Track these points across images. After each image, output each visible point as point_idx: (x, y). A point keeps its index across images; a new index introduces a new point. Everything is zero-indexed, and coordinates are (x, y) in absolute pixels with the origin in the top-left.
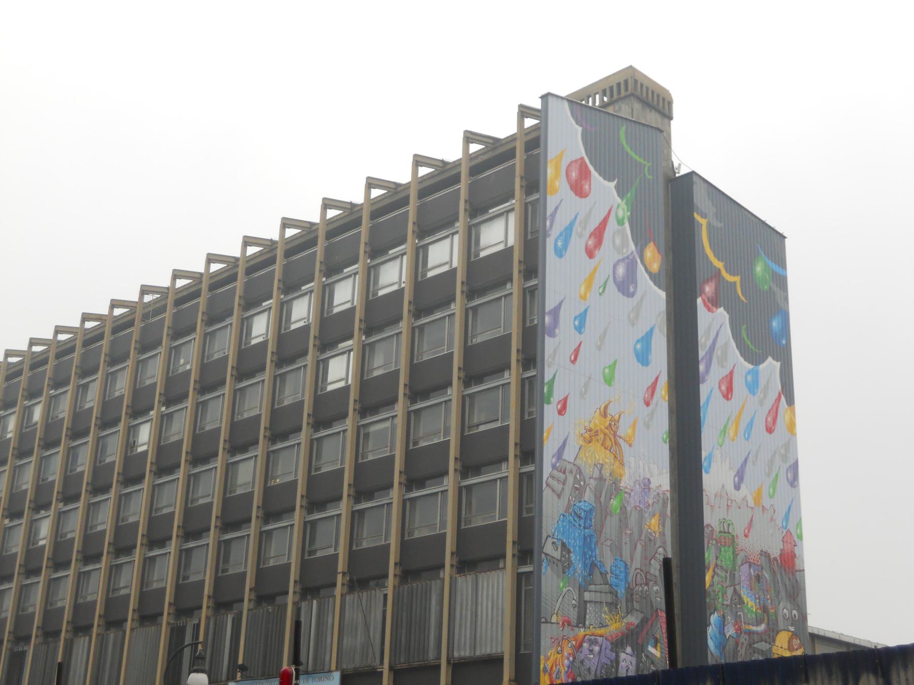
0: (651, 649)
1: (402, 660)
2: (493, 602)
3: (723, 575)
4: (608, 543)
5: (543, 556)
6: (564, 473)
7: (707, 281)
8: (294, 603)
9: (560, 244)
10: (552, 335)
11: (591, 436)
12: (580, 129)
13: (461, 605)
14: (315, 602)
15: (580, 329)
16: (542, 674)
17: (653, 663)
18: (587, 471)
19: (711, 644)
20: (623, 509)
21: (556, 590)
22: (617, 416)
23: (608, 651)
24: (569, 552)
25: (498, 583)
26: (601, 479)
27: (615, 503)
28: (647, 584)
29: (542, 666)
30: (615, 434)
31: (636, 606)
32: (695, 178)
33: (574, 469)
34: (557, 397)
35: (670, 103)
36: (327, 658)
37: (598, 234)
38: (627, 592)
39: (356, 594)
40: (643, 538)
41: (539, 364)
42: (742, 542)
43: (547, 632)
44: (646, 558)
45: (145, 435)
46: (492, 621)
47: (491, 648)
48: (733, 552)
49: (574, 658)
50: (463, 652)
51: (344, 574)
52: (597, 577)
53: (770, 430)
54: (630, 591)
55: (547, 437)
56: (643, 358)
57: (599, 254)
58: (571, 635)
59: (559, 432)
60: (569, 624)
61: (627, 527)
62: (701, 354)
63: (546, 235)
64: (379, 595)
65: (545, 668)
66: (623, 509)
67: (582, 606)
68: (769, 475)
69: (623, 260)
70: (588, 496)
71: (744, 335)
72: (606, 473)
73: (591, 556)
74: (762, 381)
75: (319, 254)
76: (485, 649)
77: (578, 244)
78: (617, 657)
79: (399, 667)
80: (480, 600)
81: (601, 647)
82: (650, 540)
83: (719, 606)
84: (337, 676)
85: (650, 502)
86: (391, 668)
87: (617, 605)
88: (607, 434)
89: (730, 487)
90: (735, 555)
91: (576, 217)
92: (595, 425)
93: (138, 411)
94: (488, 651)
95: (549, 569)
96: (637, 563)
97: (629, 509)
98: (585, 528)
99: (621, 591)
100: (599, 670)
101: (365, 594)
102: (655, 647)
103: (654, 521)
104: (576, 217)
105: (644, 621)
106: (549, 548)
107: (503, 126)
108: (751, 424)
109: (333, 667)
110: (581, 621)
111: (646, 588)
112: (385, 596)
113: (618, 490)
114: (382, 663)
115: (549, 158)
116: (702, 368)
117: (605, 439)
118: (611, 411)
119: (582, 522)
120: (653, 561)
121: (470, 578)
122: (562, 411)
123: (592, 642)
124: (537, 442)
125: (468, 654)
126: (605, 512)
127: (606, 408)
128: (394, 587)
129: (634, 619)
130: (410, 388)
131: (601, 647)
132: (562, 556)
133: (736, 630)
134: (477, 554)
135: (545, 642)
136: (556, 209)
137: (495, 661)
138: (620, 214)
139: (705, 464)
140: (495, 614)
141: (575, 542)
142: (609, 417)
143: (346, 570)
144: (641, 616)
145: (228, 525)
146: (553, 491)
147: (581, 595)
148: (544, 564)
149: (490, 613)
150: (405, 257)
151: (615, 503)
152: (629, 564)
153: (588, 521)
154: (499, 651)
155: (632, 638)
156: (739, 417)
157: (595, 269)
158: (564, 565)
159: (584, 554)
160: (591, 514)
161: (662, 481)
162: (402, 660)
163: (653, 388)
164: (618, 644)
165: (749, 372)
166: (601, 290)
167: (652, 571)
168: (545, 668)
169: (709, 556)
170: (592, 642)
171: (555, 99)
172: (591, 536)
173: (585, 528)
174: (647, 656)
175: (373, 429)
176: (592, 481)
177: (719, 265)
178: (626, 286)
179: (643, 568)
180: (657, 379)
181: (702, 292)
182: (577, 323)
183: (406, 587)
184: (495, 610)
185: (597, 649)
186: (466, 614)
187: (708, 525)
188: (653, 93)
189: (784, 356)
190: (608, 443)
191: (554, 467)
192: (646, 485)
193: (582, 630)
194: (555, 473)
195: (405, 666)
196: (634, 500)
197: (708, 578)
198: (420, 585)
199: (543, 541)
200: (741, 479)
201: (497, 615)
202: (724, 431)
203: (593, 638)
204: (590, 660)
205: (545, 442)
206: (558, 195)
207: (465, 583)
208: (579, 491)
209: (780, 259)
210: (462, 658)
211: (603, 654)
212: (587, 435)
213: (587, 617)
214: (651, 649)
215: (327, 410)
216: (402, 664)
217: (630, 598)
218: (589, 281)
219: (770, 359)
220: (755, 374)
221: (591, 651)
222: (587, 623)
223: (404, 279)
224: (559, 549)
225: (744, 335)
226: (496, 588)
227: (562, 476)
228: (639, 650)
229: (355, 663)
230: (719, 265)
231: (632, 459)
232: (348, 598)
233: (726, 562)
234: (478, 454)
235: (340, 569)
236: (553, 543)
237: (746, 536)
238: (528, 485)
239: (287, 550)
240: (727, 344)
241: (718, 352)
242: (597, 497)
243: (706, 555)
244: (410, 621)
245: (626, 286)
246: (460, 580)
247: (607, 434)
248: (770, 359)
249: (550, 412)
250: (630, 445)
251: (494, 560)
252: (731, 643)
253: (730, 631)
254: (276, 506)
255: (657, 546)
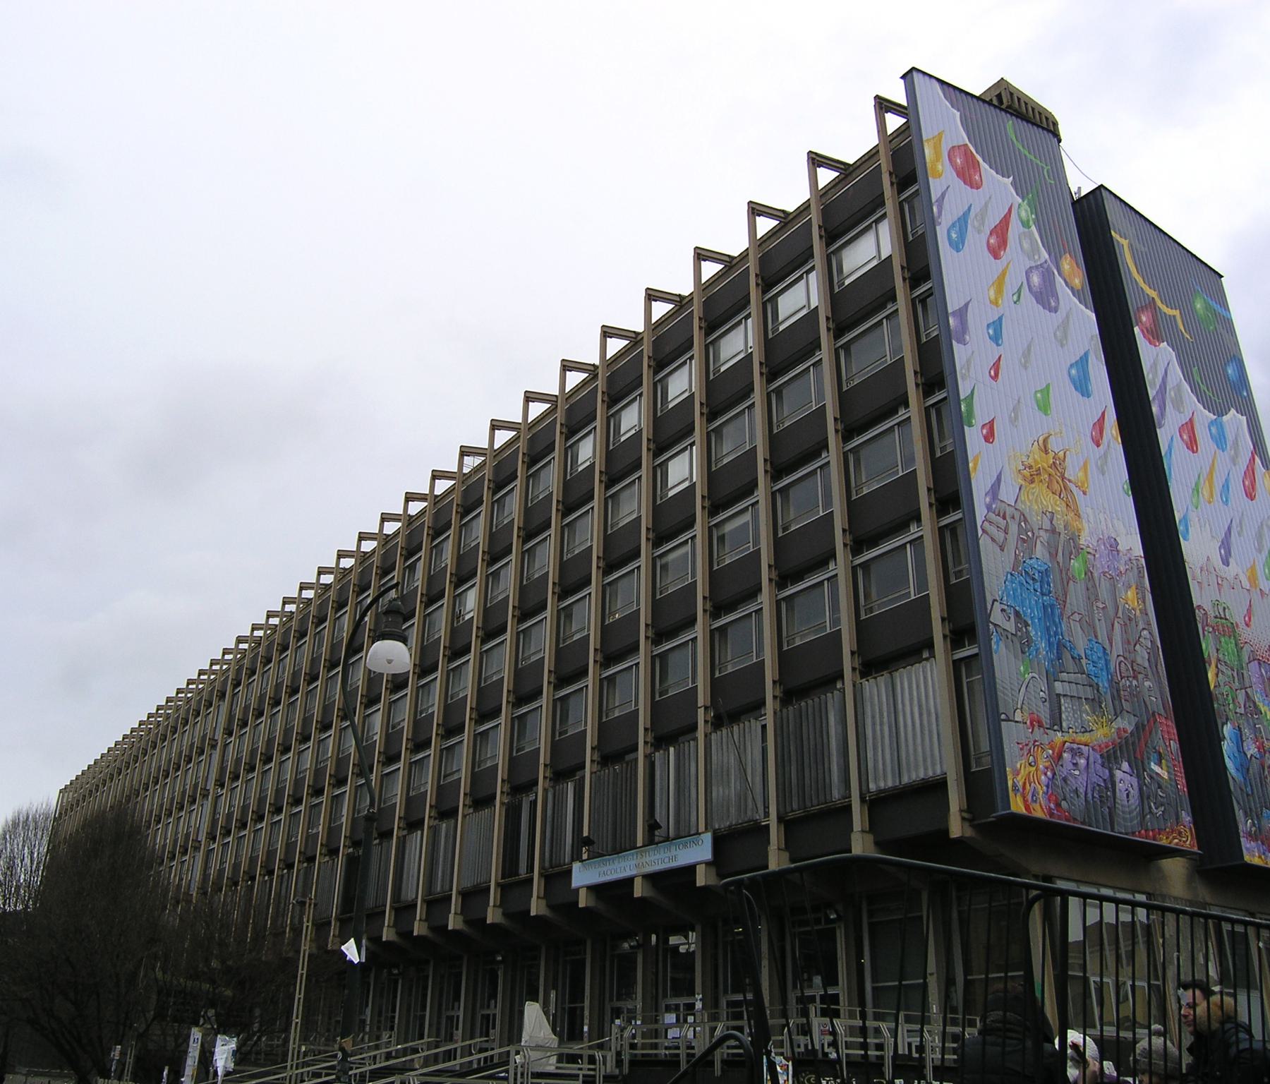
0: (1154, 767)
1: (795, 806)
2: (920, 706)
3: (1230, 673)
4: (1077, 617)
5: (991, 626)
6: (1004, 518)
7: (1142, 309)
8: (645, 756)
9: (954, 236)
10: (962, 341)
11: (1032, 475)
12: (958, 114)
13: (873, 717)
14: (672, 749)
15: (996, 338)
16: (1011, 794)
17: (1160, 787)
18: (1035, 520)
19: (1229, 764)
20: (1089, 573)
21: (1015, 674)
22: (1061, 454)
23: (1098, 767)
24: (1027, 625)
25: (925, 678)
26: (1053, 531)
27: (1076, 564)
28: (1135, 677)
29: (1010, 783)
30: (1063, 478)
31: (1126, 706)
32: (1104, 193)
33: (1017, 515)
34: (980, 418)
35: (1055, 124)
36: (693, 819)
37: (1001, 232)
38: (1111, 687)
39: (724, 731)
40: (1120, 614)
41: (949, 381)
42: (1244, 633)
43: (1012, 735)
44: (1129, 642)
45: (472, 600)
46: (922, 732)
47: (926, 769)
48: (1236, 645)
49: (1054, 774)
50: (883, 781)
51: (706, 708)
52: (1070, 665)
53: (1251, 495)
54: (1114, 685)
55: (975, 468)
56: (1082, 386)
57: (1007, 255)
58: (1046, 740)
59: (990, 467)
60: (1041, 726)
61: (1097, 599)
62: (1152, 393)
63: (933, 223)
64: (756, 726)
65: (1014, 785)
66: (1089, 573)
67: (1055, 701)
68: (1260, 551)
69: (1037, 267)
70: (1040, 551)
71: (1197, 378)
72: (1060, 526)
73: (1056, 633)
74: (1230, 437)
75: (645, 352)
76: (916, 773)
77: (977, 240)
78: (1112, 776)
79: (791, 816)
80: (900, 706)
81: (1088, 759)
82: (1130, 619)
83: (1231, 715)
84: (707, 838)
85: (1122, 569)
86: (780, 819)
87: (1100, 703)
88: (1049, 472)
89: (1217, 561)
90: (1239, 649)
91: (969, 209)
92: (1035, 461)
93: (463, 578)
94: (922, 776)
95: (1002, 645)
96: (1118, 648)
97: (1096, 575)
98: (1043, 594)
99: (1104, 684)
100: (1090, 795)
101: (736, 728)
102: (1160, 764)
103: (1131, 594)
104: (969, 209)
105: (1139, 727)
106: (997, 617)
107: (855, 139)
108: (1226, 486)
109: (702, 828)
110: (1056, 721)
111: (1135, 683)
112: (764, 727)
113: (1079, 549)
114: (767, 814)
115: (924, 138)
116: (1155, 409)
117: (1050, 480)
118: (1053, 445)
119: (1038, 585)
120: (1138, 647)
121: (883, 680)
122: (989, 437)
123: (1076, 753)
124: (962, 485)
125: (890, 784)
126: (1067, 578)
127: (1045, 441)
128: (775, 713)
129: (1126, 724)
130: (771, 463)
131: (1088, 759)
132: (1018, 629)
133: (1259, 748)
134: (889, 648)
135: (1010, 748)
136: (943, 195)
137: (936, 787)
138: (1023, 214)
139: (1181, 528)
140: (925, 722)
141: (1032, 612)
142: (1052, 454)
143: (709, 704)
144: (1134, 720)
145: (562, 680)
146: (993, 540)
147: (1050, 687)
148: (994, 640)
149: (918, 722)
150: (750, 321)
151: (1076, 564)
152: (1107, 646)
153: (1047, 583)
154: (939, 772)
155: (1128, 749)
156: (1211, 473)
157: (1003, 274)
158: (1025, 645)
159: (1048, 629)
160: (1048, 576)
161: (1132, 543)
162: (795, 806)
163: (1100, 424)
164: (1110, 757)
165: (1212, 423)
166: (1015, 298)
167: (1139, 661)
168: (1014, 785)
169: (1208, 645)
170: (1076, 753)
171: (921, 75)
172: (1052, 606)
173: (1043, 594)
174: (1151, 778)
175: (728, 527)
176: (1042, 533)
177: (1153, 294)
178: (1046, 297)
179: (1127, 655)
180: (1103, 414)
181: (1139, 322)
182: (991, 332)
183: (791, 708)
184: (925, 716)
185: (1082, 762)
186: (882, 730)
187: (1199, 607)
188: (1033, 109)
189: (1248, 408)
190: (1056, 487)
191: (989, 508)
192: (1113, 546)
193: (1059, 734)
194: (992, 516)
195: (799, 813)
196: (1101, 564)
197: (1211, 675)
198: (810, 702)
199: (989, 607)
200: (1228, 553)
201: (929, 722)
202: (1196, 490)
203: (1075, 746)
204: (1075, 777)
205: (973, 475)
206: (942, 180)
207: (875, 688)
208: (1027, 542)
209: (1219, 296)
210: (881, 791)
211: (1092, 770)
212: (1026, 472)
213: (1063, 716)
214: (1154, 767)
215: (670, 521)
216: (795, 810)
217: (1116, 696)
218: (1000, 282)
219: (1233, 411)
220: (1221, 427)
221: (1075, 765)
222: (1064, 724)
223: (750, 344)
224: (1012, 617)
225: (1197, 378)
226: (925, 685)
227: (1002, 523)
228: (1139, 768)
229: (731, 819)
230: (1153, 294)
231: (1089, 510)
232: (713, 736)
233: (1231, 659)
234: (876, 521)
235: (701, 703)
236: (1003, 610)
237: (1247, 625)
238: (957, 541)
239: (636, 693)
240: (1179, 386)
241: (1170, 394)
242: (1054, 555)
243: (1204, 646)
244: (801, 753)
245: (1046, 297)
246: (869, 686)
247: (1049, 472)
248: (1233, 411)
249: (973, 436)
250: (1085, 493)
251: (918, 650)
252: (1255, 764)
253: (1251, 750)
254: (616, 648)
255: (1141, 627)
